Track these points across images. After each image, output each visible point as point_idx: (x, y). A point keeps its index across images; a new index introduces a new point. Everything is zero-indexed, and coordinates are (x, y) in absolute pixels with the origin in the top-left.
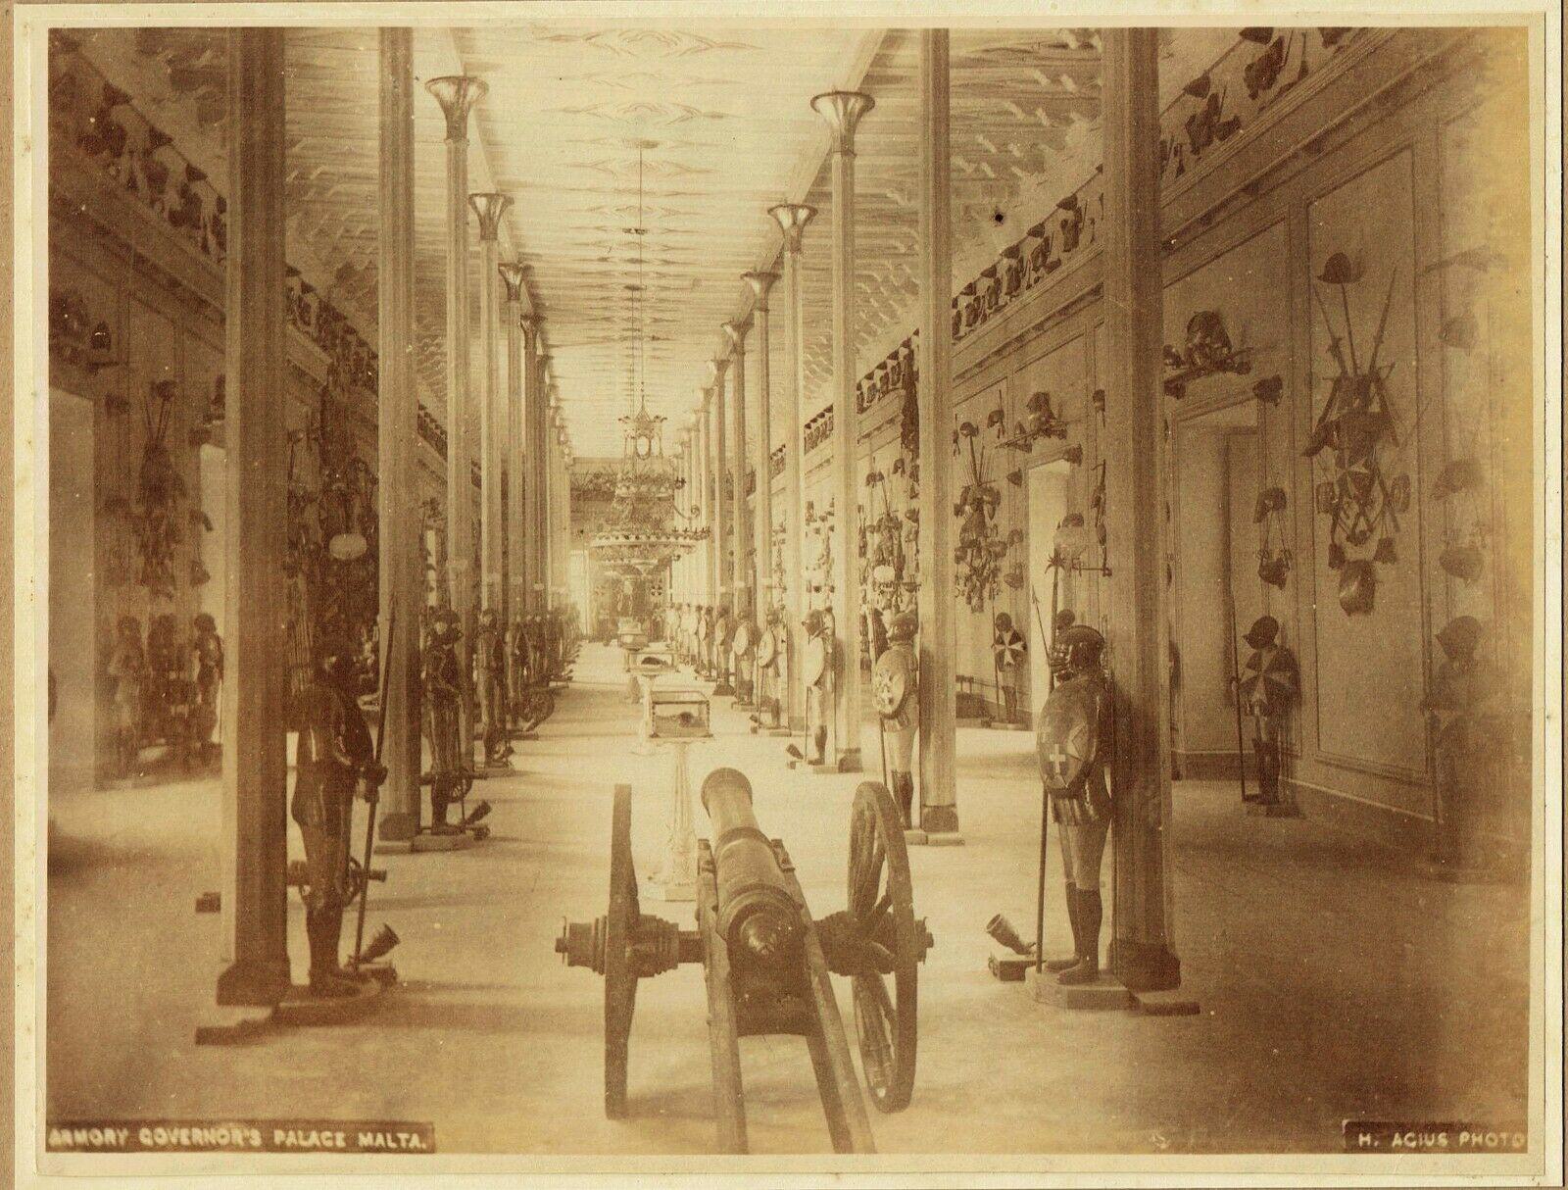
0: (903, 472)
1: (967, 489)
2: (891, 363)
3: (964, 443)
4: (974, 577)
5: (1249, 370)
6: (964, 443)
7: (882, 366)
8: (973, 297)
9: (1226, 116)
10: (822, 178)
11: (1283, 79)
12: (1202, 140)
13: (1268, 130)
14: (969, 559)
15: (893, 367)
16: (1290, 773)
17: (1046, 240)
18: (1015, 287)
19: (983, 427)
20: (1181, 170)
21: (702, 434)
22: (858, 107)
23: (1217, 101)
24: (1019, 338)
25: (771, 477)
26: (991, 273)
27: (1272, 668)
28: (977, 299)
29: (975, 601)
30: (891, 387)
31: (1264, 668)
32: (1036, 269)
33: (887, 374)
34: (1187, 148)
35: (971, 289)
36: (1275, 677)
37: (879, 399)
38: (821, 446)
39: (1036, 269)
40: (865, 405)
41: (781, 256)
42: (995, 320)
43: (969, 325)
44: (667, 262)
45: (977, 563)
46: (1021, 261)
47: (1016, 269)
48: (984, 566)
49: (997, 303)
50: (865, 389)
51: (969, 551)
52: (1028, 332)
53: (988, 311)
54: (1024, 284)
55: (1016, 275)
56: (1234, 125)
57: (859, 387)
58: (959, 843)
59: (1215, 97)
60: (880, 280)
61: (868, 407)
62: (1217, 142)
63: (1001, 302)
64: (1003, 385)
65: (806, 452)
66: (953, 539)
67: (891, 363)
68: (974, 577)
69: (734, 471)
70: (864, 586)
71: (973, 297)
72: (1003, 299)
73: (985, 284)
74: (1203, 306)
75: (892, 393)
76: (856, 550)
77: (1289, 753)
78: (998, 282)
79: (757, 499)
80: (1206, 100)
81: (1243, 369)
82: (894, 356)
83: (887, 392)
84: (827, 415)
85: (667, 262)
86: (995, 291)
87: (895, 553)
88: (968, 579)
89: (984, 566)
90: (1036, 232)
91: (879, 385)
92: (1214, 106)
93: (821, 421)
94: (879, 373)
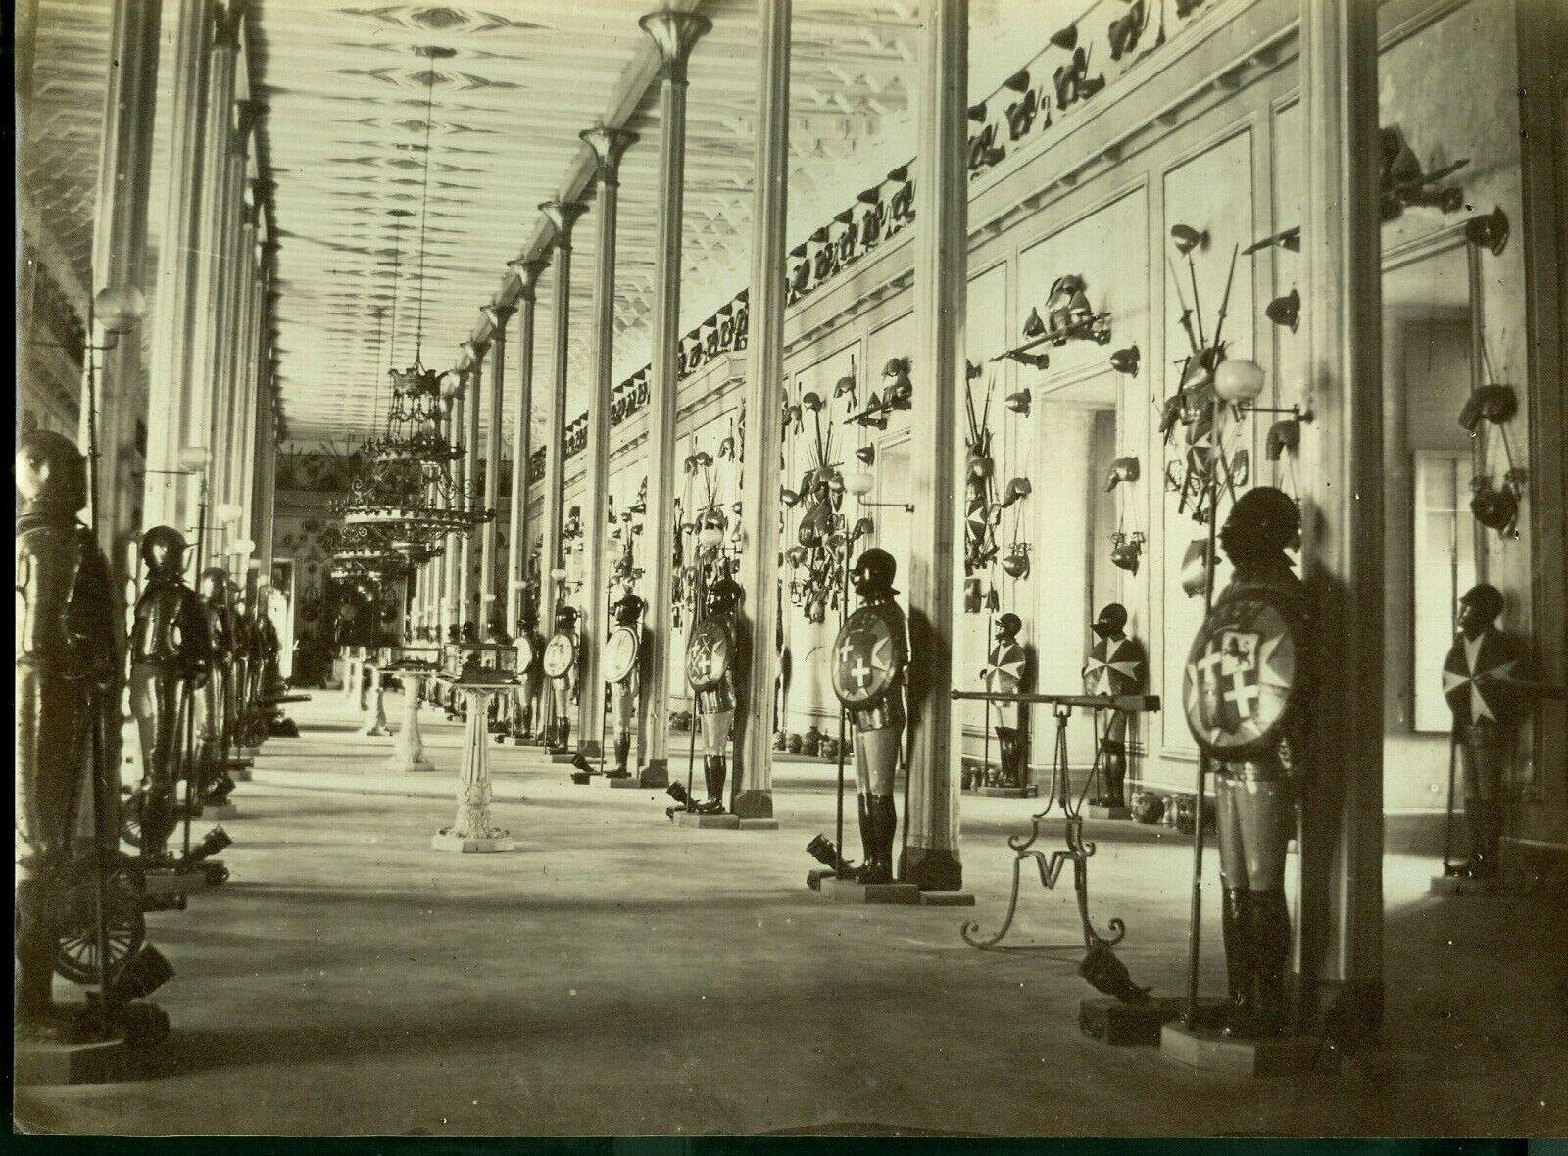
0: (732, 454)
1: (810, 474)
2: (722, 319)
3: (809, 416)
4: (815, 583)
5: (1107, 340)
6: (809, 416)
7: (712, 322)
8: (824, 245)
9: (1092, 74)
10: (647, 100)
11: (1146, 40)
12: (1020, 129)
13: (719, 391)
14: (809, 562)
15: (725, 325)
16: (1135, 771)
17: (909, 186)
18: (870, 238)
19: (831, 400)
20: (1048, 123)
21: (468, 404)
22: (693, 29)
23: (1083, 57)
24: (877, 294)
25: (565, 456)
26: (846, 217)
27: (1117, 658)
28: (829, 247)
29: (814, 610)
30: (719, 349)
31: (1108, 660)
32: (897, 217)
33: (716, 332)
34: (1054, 101)
35: (822, 235)
36: (1117, 666)
37: (706, 362)
38: (626, 422)
39: (897, 217)
40: (687, 369)
41: (592, 184)
42: (847, 273)
43: (819, 276)
44: (445, 185)
45: (819, 565)
46: (880, 206)
47: (875, 215)
48: (827, 568)
49: (851, 252)
50: (688, 350)
51: (810, 551)
52: (886, 287)
53: (841, 262)
54: (883, 231)
55: (873, 222)
56: (1099, 85)
57: (681, 347)
58: (773, 826)
59: (1032, 93)
60: (712, 219)
61: (690, 374)
62: (1081, 100)
63: (857, 253)
64: (855, 349)
65: (544, 448)
66: (789, 538)
67: (722, 319)
68: (815, 583)
69: (489, 458)
70: (678, 604)
71: (824, 245)
72: (859, 248)
73: (838, 231)
74: (1065, 270)
75: (722, 356)
76: (669, 561)
77: (1136, 753)
78: (853, 229)
79: (546, 486)
80: (1024, 95)
81: (1105, 338)
82: (727, 310)
83: (717, 353)
84: (637, 382)
85: (445, 185)
86: (849, 238)
87: (722, 864)
88: (808, 586)
89: (827, 568)
90: (899, 174)
91: (705, 346)
92: (1080, 61)
93: (628, 390)
94: (707, 331)
